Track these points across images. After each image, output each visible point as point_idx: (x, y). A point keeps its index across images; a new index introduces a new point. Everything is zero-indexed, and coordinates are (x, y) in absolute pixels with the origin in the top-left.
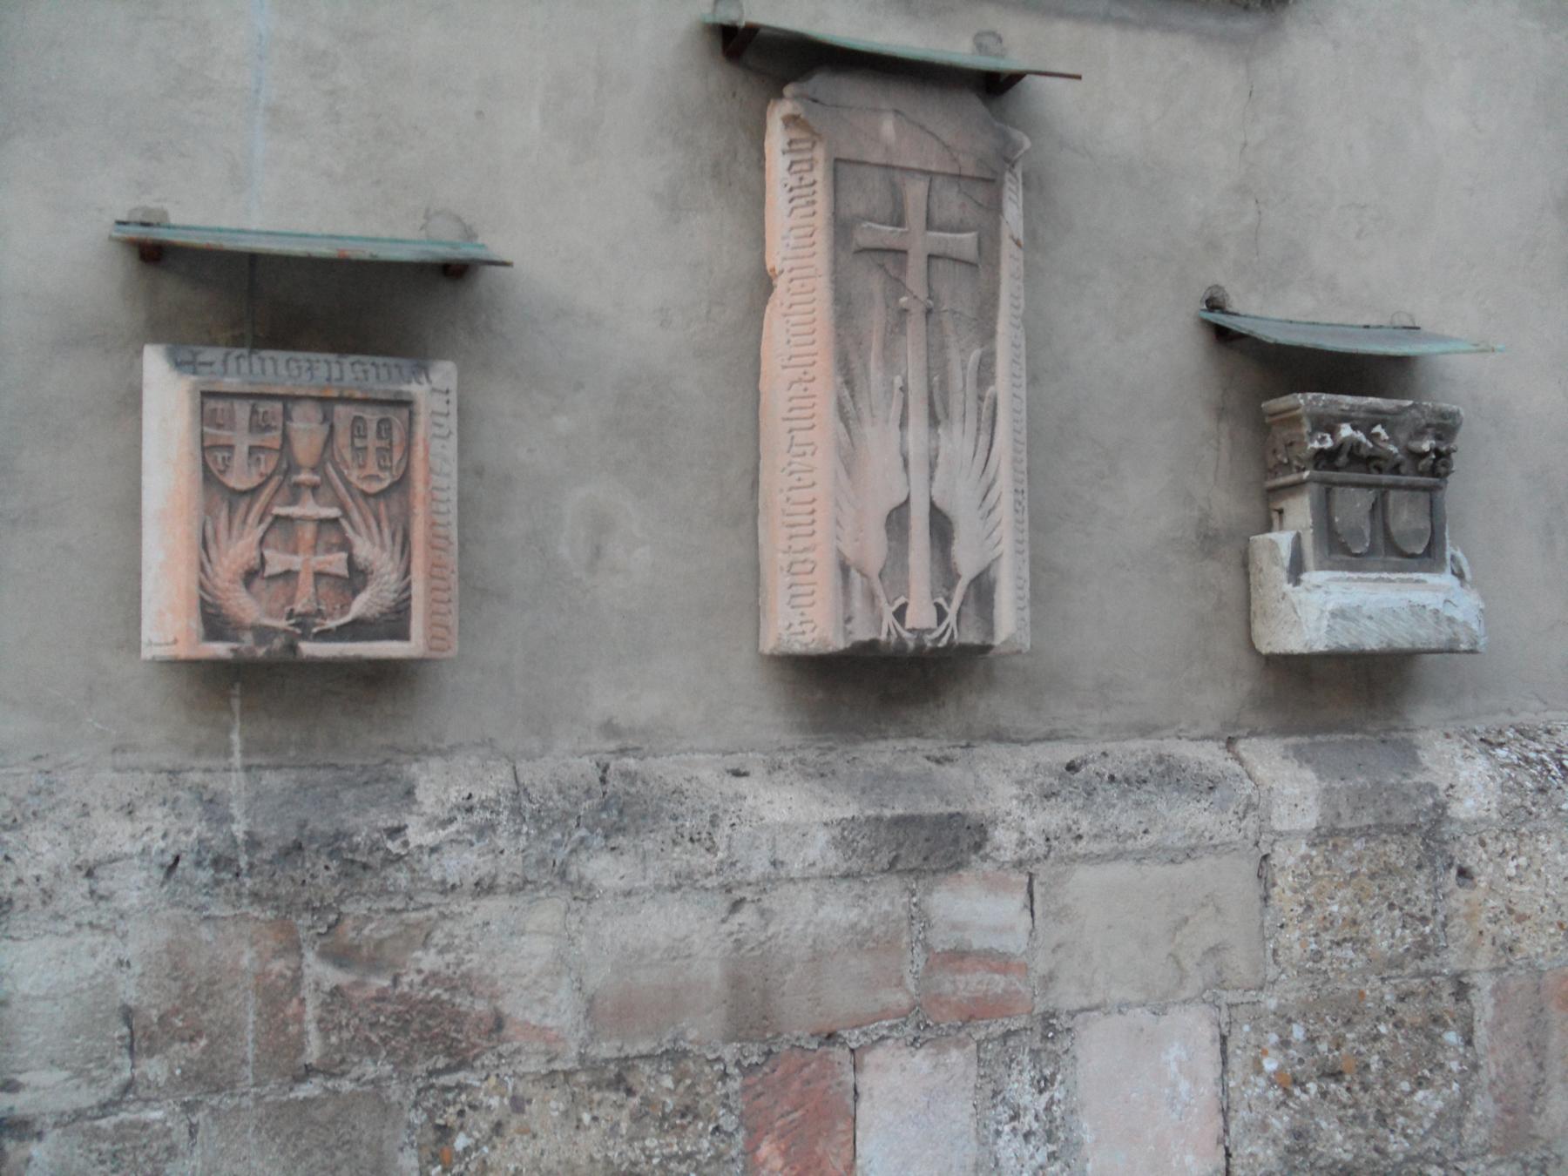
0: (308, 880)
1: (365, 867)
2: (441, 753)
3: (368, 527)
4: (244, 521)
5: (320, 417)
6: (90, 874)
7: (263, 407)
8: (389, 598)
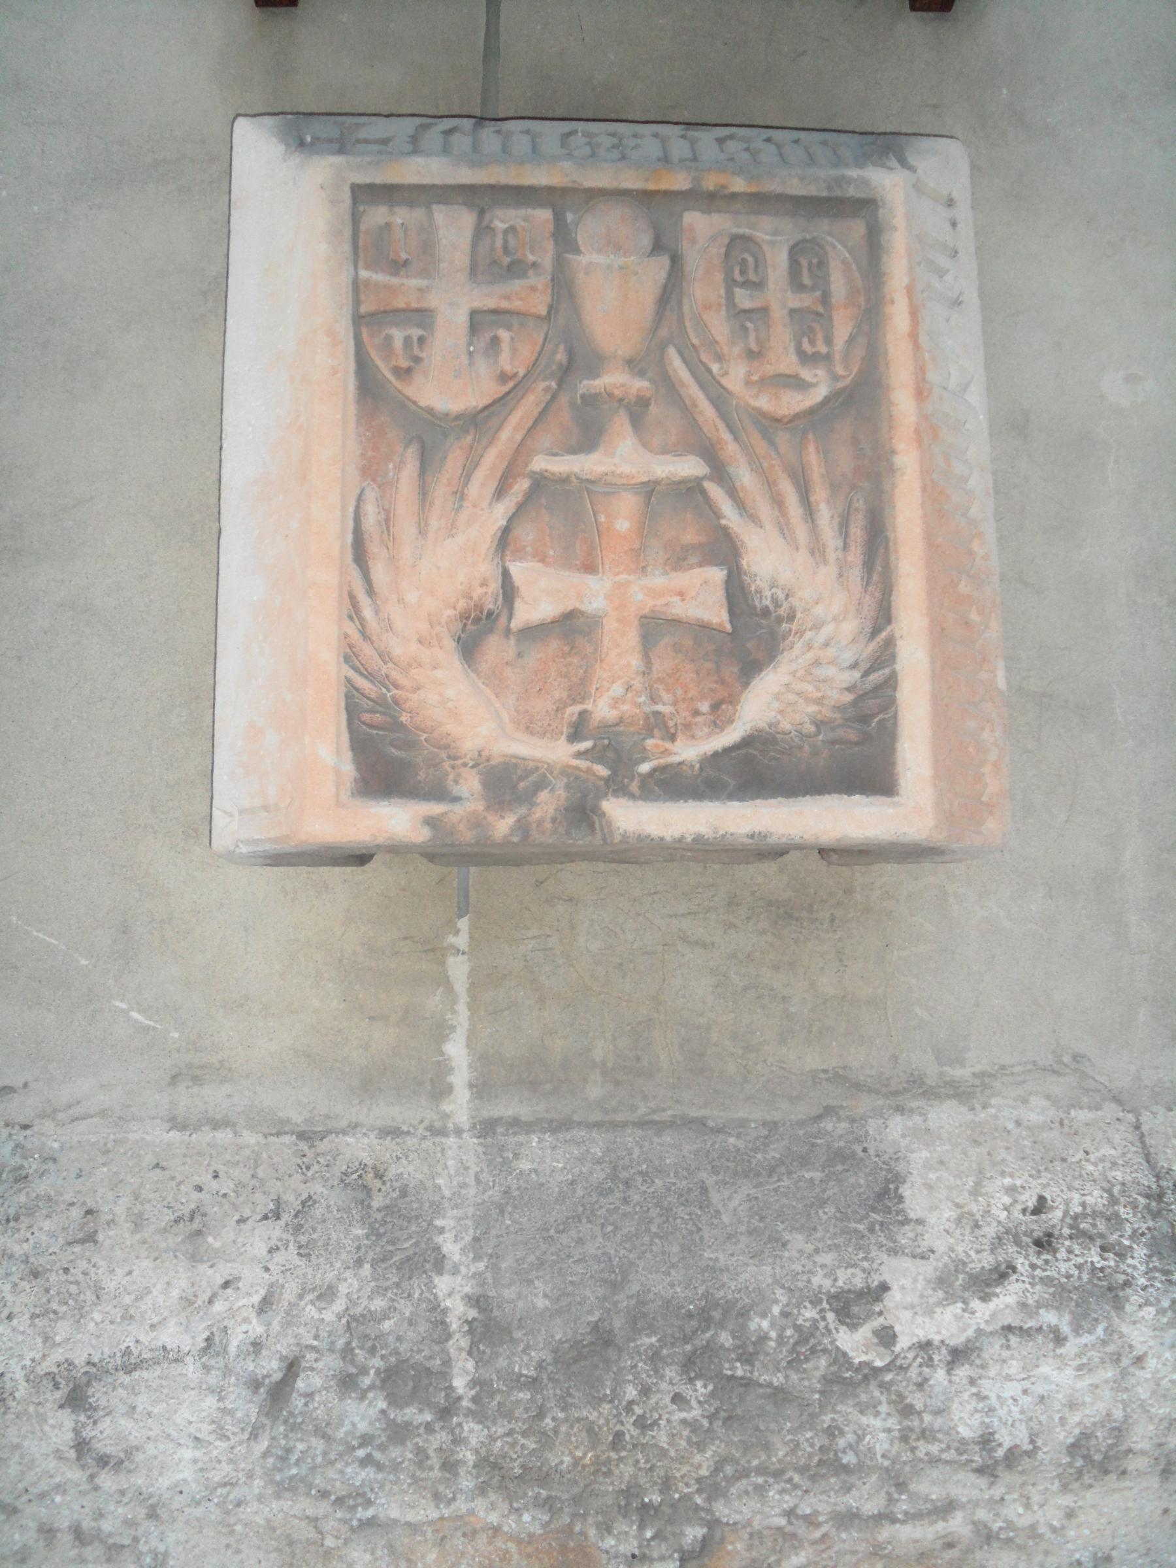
0: (630, 1431)
1: (780, 1395)
2: (960, 1093)
3: (778, 502)
4: (460, 494)
5: (646, 241)
6: (76, 1399)
7: (503, 218)
8: (838, 681)
